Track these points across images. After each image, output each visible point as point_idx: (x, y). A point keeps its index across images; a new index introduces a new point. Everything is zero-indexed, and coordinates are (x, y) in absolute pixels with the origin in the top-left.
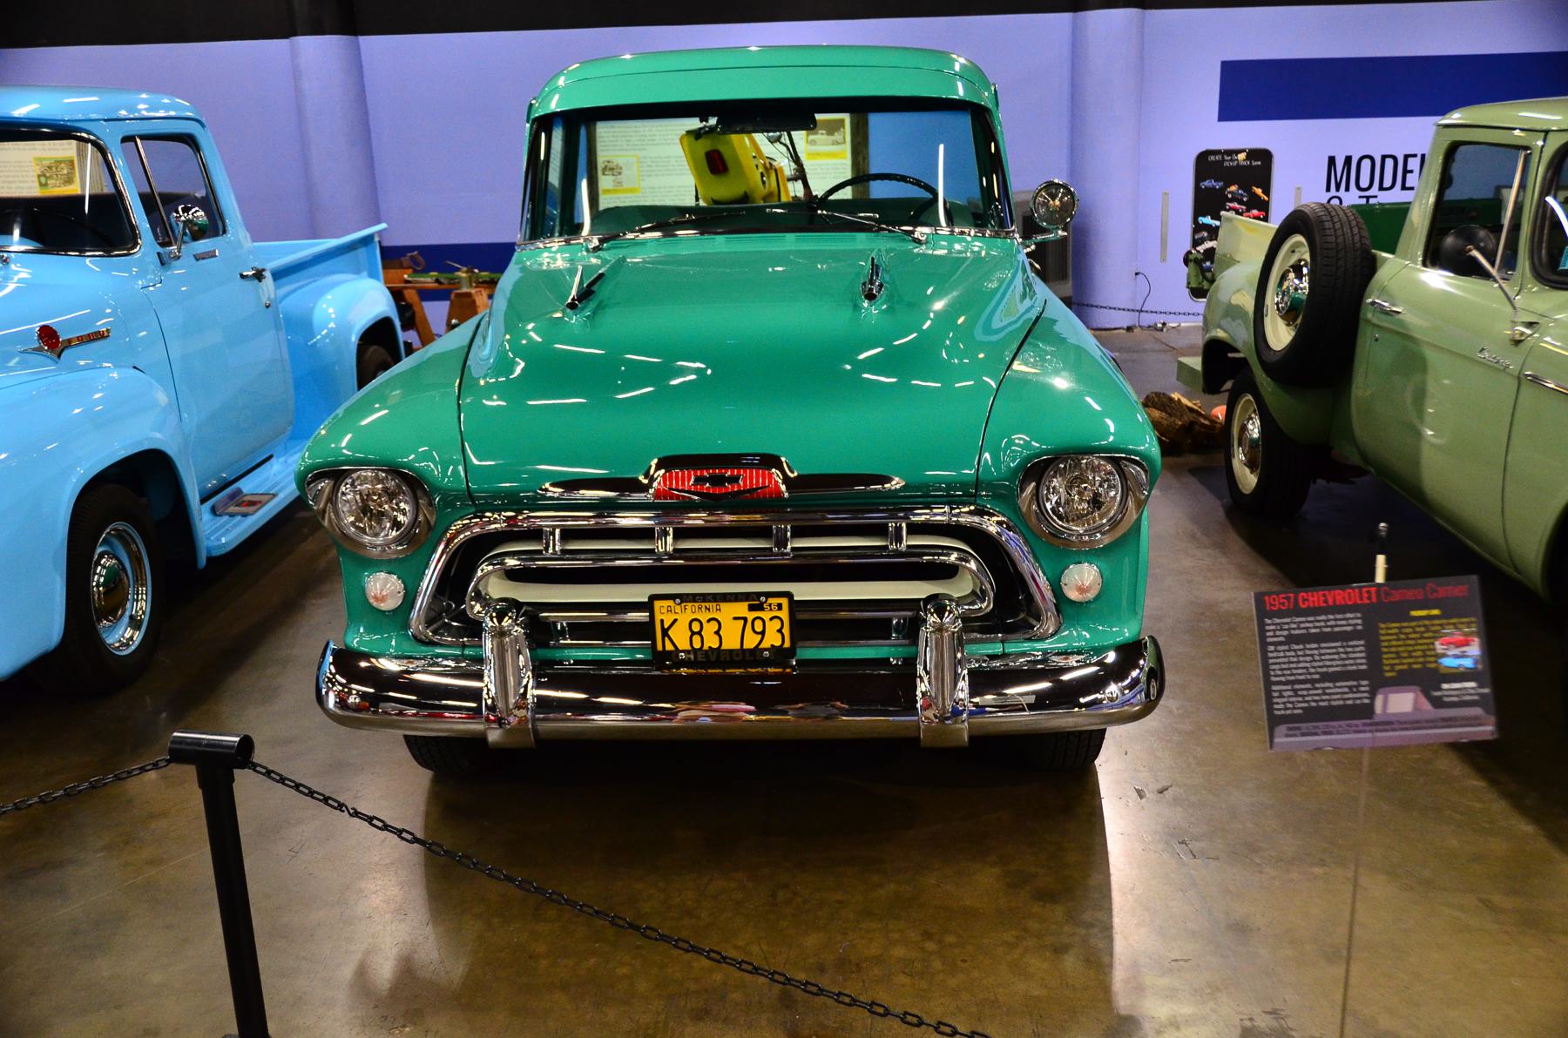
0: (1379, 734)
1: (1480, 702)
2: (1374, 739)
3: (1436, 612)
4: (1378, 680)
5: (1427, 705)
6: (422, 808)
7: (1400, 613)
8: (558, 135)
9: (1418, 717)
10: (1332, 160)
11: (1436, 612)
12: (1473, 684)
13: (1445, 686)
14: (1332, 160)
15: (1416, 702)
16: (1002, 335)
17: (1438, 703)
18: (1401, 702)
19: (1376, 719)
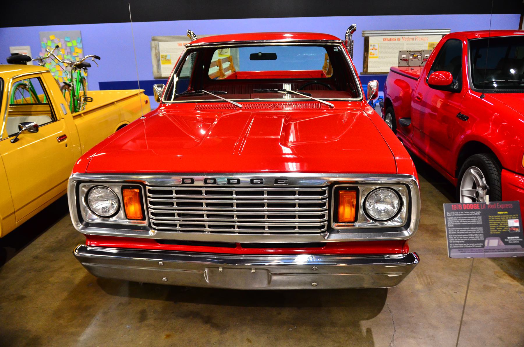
0: (486, 253)
1: (520, 243)
2: (484, 255)
3: (506, 213)
4: (488, 234)
5: (502, 244)
6: (138, 299)
7: (494, 212)
8: (275, 278)
9: (499, 248)
10: (75, 117)
11: (506, 213)
12: (518, 237)
13: (509, 238)
14: (75, 117)
15: (499, 243)
16: (468, 160)
17: (506, 243)
18: (494, 243)
19: (485, 248)
